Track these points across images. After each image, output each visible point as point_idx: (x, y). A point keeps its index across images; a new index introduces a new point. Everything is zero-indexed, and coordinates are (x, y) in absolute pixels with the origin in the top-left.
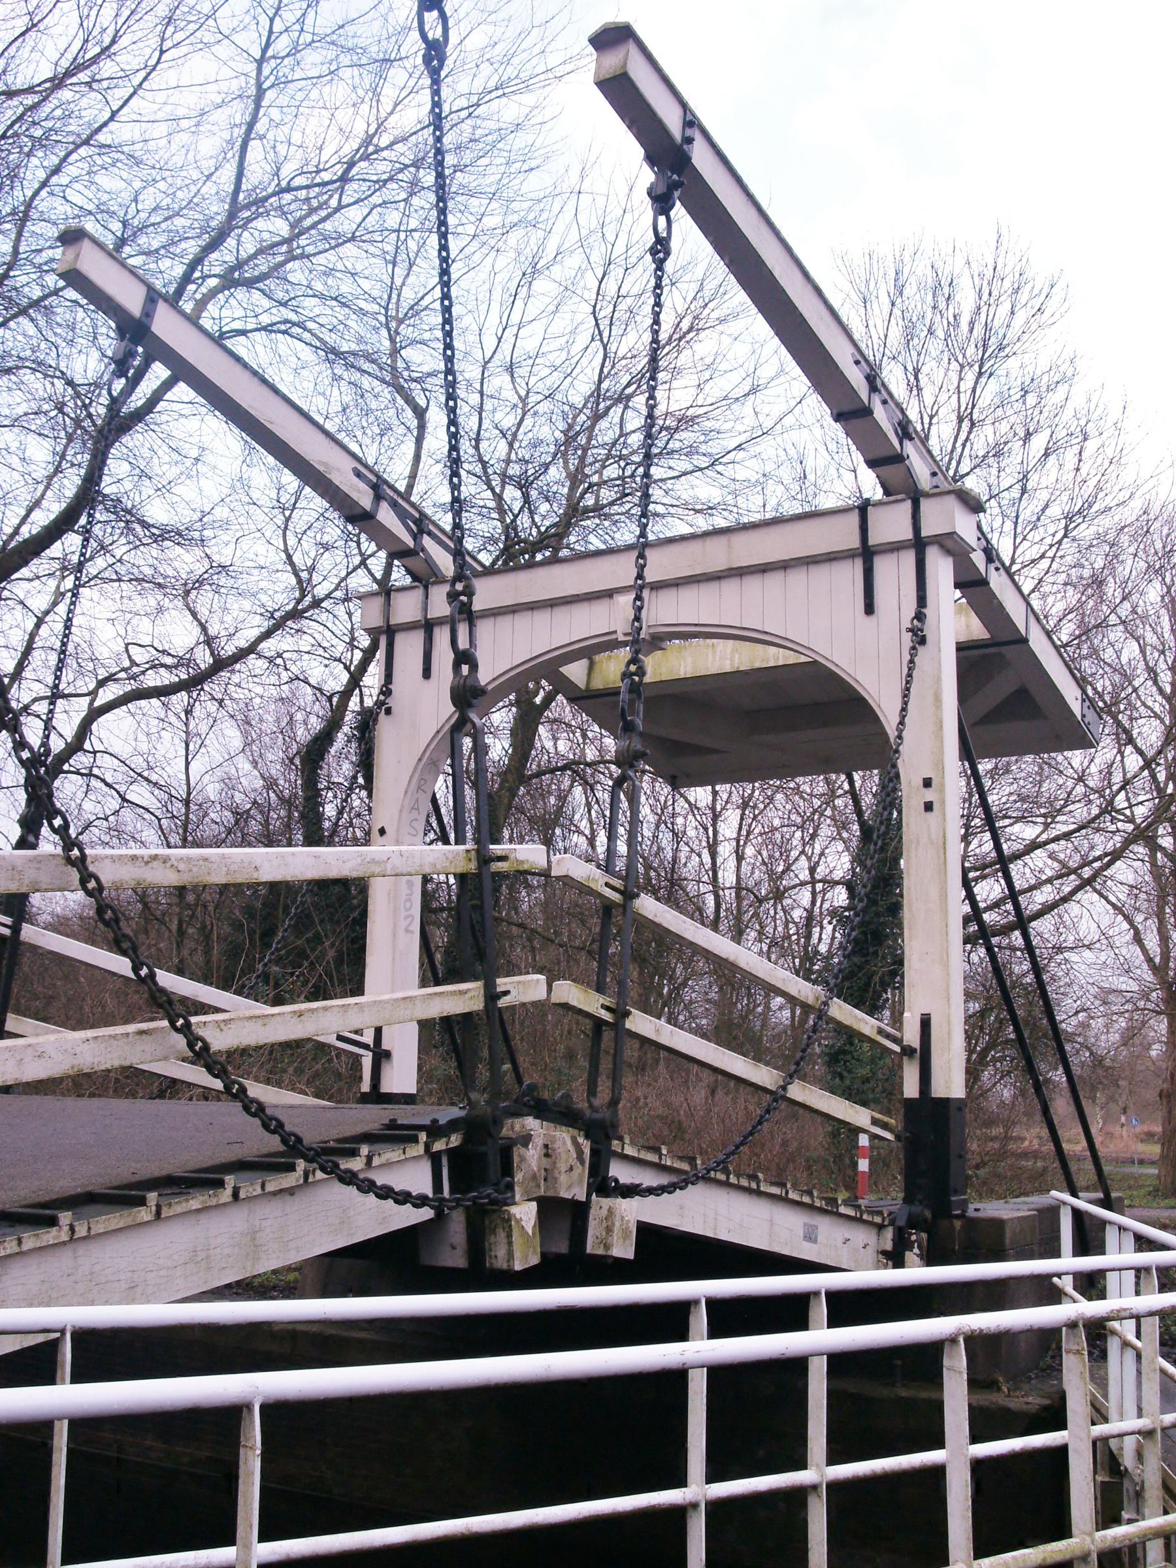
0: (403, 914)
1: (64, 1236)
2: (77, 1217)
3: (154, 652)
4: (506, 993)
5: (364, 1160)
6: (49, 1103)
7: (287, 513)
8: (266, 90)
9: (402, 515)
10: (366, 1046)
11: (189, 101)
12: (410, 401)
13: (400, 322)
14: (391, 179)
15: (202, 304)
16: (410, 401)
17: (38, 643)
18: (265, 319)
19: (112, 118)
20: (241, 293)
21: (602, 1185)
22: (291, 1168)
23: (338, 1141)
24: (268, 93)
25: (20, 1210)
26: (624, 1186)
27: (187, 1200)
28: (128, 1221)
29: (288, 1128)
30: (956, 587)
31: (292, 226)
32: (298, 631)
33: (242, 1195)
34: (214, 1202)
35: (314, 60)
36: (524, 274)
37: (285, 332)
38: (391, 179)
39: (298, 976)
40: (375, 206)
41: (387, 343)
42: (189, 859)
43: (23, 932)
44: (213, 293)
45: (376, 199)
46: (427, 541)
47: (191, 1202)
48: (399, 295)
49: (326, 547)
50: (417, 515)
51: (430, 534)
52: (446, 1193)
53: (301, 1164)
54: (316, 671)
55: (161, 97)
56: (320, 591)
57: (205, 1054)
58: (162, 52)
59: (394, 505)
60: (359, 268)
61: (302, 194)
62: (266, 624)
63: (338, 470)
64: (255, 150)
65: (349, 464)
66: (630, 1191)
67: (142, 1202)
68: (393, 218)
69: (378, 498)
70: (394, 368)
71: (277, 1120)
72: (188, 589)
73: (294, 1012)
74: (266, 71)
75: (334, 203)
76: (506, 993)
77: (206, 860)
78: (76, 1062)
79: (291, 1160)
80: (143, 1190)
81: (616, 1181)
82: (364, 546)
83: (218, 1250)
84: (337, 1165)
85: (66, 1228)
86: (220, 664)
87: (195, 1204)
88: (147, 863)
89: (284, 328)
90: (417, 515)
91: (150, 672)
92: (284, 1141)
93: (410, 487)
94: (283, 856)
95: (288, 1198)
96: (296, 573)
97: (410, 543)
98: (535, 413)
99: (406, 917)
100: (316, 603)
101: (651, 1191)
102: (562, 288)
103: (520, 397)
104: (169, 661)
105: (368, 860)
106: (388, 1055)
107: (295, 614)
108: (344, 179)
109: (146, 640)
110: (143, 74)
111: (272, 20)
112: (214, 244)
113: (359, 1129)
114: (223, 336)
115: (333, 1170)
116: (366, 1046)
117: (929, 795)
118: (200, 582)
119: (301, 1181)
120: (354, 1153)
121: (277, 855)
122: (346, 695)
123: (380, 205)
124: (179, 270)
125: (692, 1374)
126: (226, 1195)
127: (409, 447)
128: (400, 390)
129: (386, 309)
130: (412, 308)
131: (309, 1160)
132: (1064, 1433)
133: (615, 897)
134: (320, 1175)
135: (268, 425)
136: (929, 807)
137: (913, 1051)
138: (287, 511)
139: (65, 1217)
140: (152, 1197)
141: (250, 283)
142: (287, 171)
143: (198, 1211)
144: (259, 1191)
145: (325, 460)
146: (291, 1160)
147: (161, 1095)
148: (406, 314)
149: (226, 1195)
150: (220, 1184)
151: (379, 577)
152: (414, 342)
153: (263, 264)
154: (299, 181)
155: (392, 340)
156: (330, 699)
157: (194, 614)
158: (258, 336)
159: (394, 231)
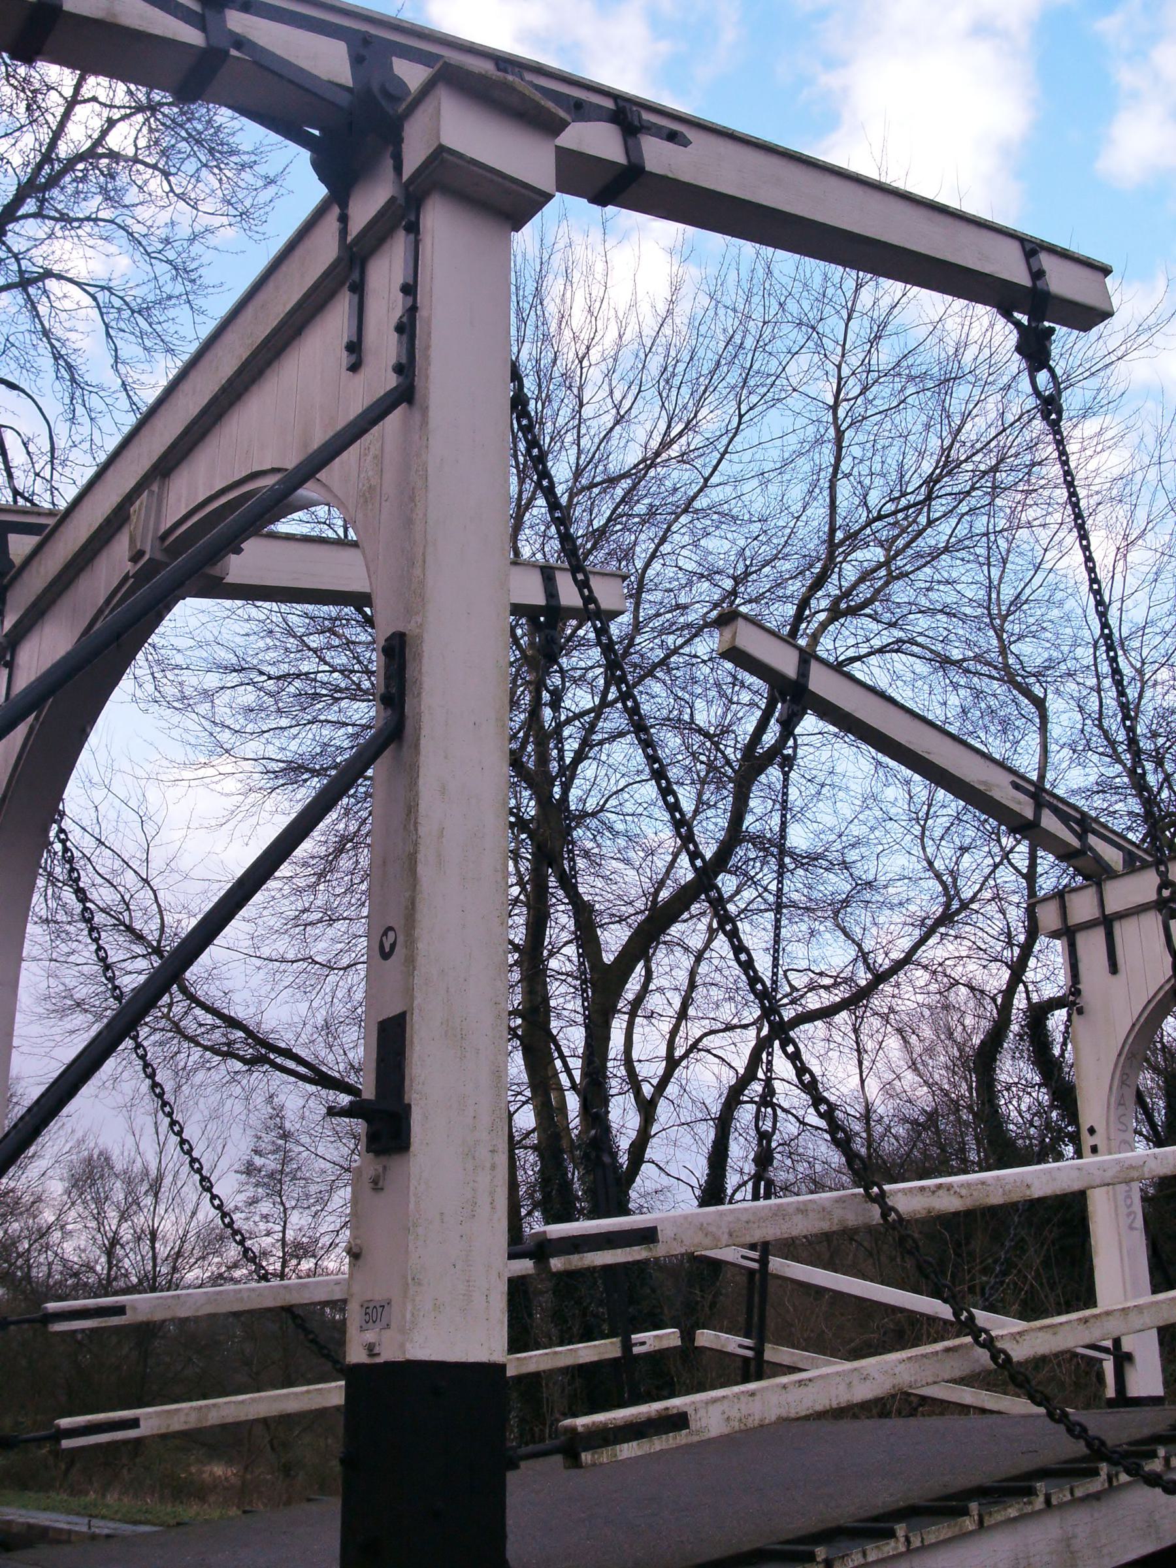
0: (1125, 1211)
1: (902, 1549)
2: (910, 1529)
3: (812, 975)
5: (1162, 1461)
6: (846, 1425)
7: (922, 823)
8: (844, 432)
9: (1064, 818)
10: (1105, 1350)
11: (772, 456)
12: (1027, 693)
13: (1004, 618)
14: (973, 488)
15: (815, 638)
16: (1027, 693)
17: (699, 980)
18: (877, 643)
19: (705, 485)
20: (851, 623)
22: (1095, 1473)
23: (1130, 1444)
24: (846, 434)
25: (778, 1547)
27: (1005, 1509)
28: (956, 1531)
31: (888, 550)
32: (956, 937)
33: (1054, 1501)
34: (1029, 1509)
35: (882, 394)
36: (1118, 549)
37: (897, 651)
38: (973, 488)
39: (1008, 1284)
40: (963, 515)
41: (995, 642)
42: (968, 1185)
43: (770, 1265)
44: (824, 626)
45: (963, 508)
46: (1092, 840)
47: (1010, 1510)
48: (998, 593)
49: (964, 849)
50: (1078, 816)
51: (1095, 832)
53: (1104, 1468)
54: (972, 970)
55: (747, 456)
56: (967, 894)
57: (1008, 1366)
58: (741, 416)
59: (1056, 811)
60: (954, 575)
61: (891, 520)
62: (917, 933)
63: (998, 786)
64: (844, 489)
65: (1005, 779)
67: (965, 1512)
68: (981, 523)
69: (1039, 805)
70: (1007, 666)
71: (1080, 1425)
72: (838, 908)
73: (1080, 1320)
74: (841, 413)
75: (923, 520)
77: (983, 1183)
78: (896, 1382)
79: (1092, 1465)
80: (888, 1521)
82: (1004, 840)
83: (1038, 1558)
84: (1139, 1466)
85: (902, 1539)
86: (880, 978)
87: (1012, 1512)
88: (934, 1192)
89: (897, 647)
90: (1078, 816)
91: (809, 994)
92: (1089, 1445)
93: (1042, 777)
94: (1050, 1171)
95: (1095, 1504)
96: (938, 876)
97: (1075, 842)
98: (1154, 685)
99: (1129, 1215)
100: (964, 906)
102: (1158, 555)
103: (1136, 670)
104: (827, 981)
105: (1126, 1165)
106: (1129, 1357)
107: (946, 919)
108: (929, 498)
109: (804, 964)
110: (725, 440)
111: (839, 367)
112: (819, 582)
113: (1146, 1432)
114: (841, 664)
115: (1135, 1472)
116: (1105, 1350)
118: (846, 902)
119: (1106, 1485)
120: (1153, 1455)
121: (1044, 1171)
122: (1009, 992)
123: (966, 513)
124: (790, 610)
126: (1039, 1502)
127: (1033, 739)
128: (1018, 687)
129: (988, 609)
130: (1011, 604)
131: (1112, 1462)
134: (1124, 1478)
135: (927, 756)
138: (922, 819)
139: (900, 1529)
140: (974, 1506)
141: (854, 611)
142: (874, 498)
143: (1015, 1519)
144: (1069, 1497)
145: (984, 779)
146: (1092, 1465)
147: (913, 1413)
148: (1008, 610)
149: (1039, 1502)
150: (1030, 1492)
151: (1025, 871)
152: (1021, 637)
153: (865, 592)
154: (890, 507)
155: (1000, 638)
156: (994, 999)
157: (847, 935)
158: (873, 660)
159: (984, 535)
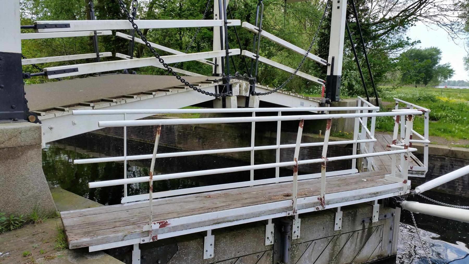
4: (231, 53)
21: (252, 93)
26: (257, 93)
29: (186, 81)
30: (119, 202)
43: (135, 39)
52: (218, 93)
66: (258, 94)
76: (231, 53)
81: (255, 92)
101: (263, 94)
117: (338, 5)
125: (353, 160)
132: (323, 143)
133: (257, 32)
136: (338, 8)
137: (330, 65)
